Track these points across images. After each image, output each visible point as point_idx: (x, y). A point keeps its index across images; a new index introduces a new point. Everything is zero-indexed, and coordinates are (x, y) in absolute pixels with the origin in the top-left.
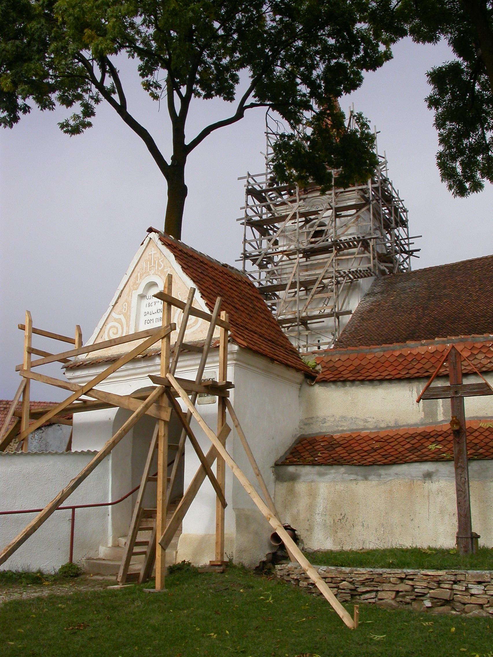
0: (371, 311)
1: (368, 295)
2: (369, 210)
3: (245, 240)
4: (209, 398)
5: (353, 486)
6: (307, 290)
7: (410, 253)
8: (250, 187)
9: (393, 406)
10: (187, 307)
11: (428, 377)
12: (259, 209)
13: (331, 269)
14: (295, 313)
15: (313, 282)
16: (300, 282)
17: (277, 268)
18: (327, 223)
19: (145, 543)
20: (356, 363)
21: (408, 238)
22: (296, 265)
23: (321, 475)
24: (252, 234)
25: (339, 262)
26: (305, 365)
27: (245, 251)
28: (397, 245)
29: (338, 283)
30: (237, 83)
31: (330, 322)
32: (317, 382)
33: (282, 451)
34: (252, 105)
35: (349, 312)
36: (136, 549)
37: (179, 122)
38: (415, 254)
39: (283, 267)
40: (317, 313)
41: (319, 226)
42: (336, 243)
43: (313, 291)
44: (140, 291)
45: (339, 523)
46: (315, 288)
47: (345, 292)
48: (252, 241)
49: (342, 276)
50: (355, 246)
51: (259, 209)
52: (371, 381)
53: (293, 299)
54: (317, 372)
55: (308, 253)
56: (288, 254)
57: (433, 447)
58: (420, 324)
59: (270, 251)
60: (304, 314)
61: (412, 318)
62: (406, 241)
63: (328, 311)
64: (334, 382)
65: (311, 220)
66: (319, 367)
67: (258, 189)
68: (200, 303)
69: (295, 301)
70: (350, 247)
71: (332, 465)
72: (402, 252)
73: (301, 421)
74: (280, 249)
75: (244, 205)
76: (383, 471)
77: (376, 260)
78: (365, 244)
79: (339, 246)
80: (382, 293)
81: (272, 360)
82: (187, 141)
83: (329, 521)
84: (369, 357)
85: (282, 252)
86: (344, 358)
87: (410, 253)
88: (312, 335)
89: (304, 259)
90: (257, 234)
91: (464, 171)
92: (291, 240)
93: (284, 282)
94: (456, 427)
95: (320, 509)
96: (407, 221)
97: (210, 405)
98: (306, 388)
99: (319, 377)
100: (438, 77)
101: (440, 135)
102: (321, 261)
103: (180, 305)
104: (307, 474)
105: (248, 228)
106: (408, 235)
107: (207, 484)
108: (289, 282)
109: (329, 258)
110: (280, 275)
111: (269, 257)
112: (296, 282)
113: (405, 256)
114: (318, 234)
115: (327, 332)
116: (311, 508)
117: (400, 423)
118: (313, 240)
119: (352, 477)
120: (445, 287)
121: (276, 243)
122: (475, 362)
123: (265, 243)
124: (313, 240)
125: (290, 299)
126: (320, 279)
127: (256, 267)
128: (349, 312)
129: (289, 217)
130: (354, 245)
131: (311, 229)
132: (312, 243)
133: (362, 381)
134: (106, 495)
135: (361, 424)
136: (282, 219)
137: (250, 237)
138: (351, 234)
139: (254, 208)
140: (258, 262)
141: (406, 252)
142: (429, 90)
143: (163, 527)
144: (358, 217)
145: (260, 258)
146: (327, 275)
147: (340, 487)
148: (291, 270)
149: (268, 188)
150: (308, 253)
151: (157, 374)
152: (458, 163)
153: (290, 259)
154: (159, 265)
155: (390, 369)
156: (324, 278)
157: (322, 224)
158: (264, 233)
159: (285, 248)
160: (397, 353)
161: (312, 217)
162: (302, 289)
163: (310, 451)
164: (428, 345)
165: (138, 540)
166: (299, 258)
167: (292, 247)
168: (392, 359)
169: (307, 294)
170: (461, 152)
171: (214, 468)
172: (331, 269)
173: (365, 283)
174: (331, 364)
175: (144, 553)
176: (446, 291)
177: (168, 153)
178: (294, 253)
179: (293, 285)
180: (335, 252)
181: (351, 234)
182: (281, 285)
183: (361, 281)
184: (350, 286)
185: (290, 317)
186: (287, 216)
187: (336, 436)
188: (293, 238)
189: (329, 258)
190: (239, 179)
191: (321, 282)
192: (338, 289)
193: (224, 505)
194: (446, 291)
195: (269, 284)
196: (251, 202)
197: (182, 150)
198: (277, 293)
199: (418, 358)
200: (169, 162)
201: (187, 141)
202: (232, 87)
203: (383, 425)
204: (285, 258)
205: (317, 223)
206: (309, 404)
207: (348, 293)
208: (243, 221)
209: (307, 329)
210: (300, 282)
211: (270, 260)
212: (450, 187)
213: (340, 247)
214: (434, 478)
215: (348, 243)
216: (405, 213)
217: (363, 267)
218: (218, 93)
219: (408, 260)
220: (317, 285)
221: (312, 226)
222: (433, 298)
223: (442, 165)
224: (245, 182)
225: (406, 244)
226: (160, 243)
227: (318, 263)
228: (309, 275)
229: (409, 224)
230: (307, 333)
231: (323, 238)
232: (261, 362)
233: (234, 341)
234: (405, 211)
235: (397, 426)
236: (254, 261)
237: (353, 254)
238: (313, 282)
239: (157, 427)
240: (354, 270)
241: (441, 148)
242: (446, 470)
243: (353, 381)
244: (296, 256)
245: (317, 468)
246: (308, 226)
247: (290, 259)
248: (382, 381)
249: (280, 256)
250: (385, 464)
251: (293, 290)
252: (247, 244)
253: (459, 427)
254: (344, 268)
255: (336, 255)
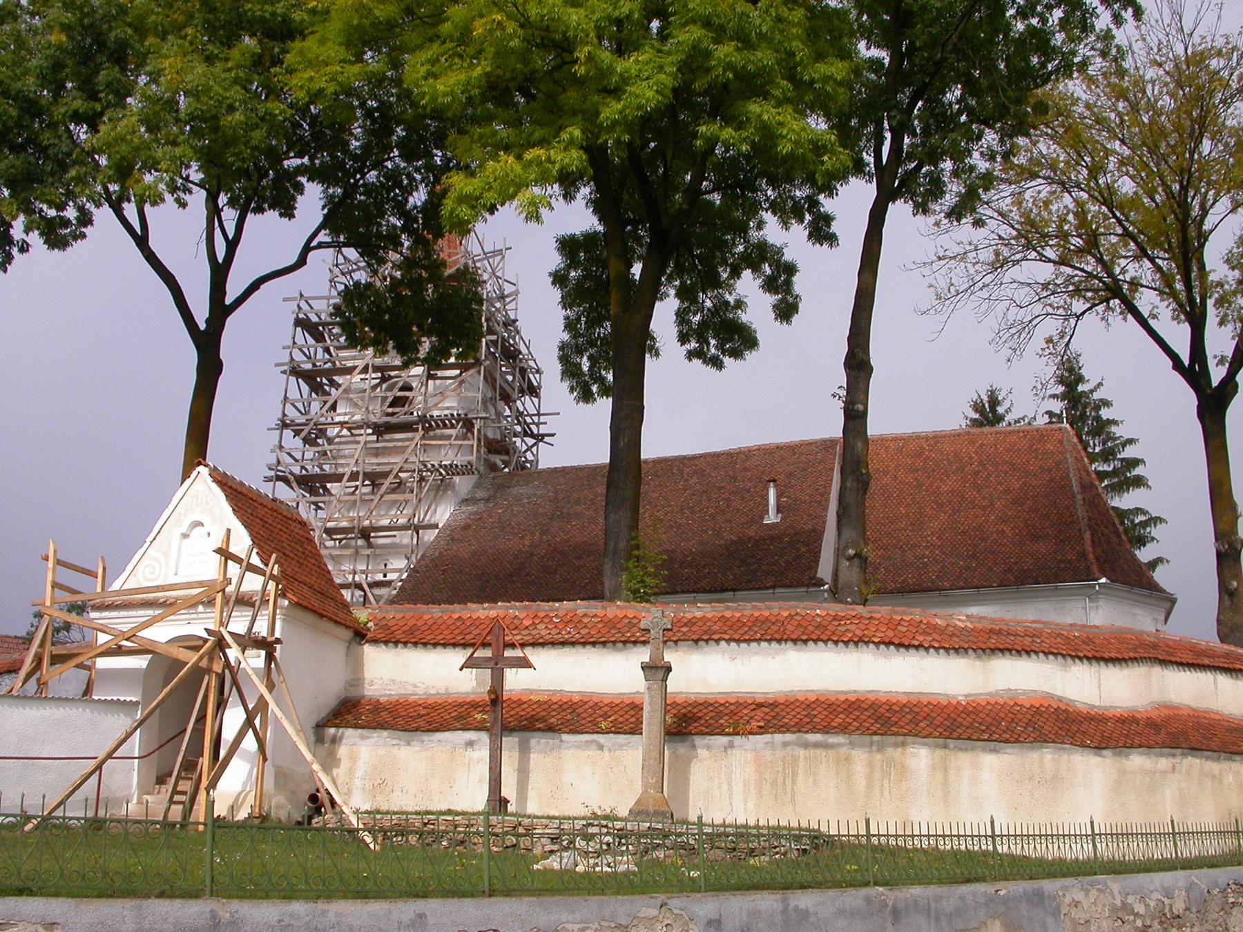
0: (466, 527)
1: (465, 501)
2: (479, 372)
3: (286, 398)
4: (255, 651)
5: (395, 750)
6: (375, 485)
7: (540, 438)
8: (301, 316)
9: (440, 672)
10: (245, 564)
11: (473, 645)
12: (312, 350)
13: (413, 459)
14: (352, 520)
15: (385, 475)
16: (365, 474)
17: (332, 447)
18: (414, 385)
19: (184, 793)
20: (411, 623)
21: (539, 414)
22: (361, 446)
23: (363, 738)
24: (298, 389)
25: (426, 448)
26: (356, 620)
27: (284, 415)
28: (519, 423)
29: (422, 479)
30: (302, 194)
31: (405, 538)
32: (367, 642)
33: (324, 713)
34: (320, 246)
35: (436, 526)
36: (177, 798)
37: (220, 272)
38: (546, 439)
39: (342, 447)
40: (385, 522)
41: (401, 389)
42: (423, 419)
43: (384, 488)
44: (184, 529)
45: (380, 786)
46: (387, 483)
47: (432, 494)
48: (297, 401)
49: (428, 470)
50: (453, 426)
51: (312, 350)
52: (425, 644)
53: (352, 498)
54: (369, 630)
55: (381, 430)
56: (351, 427)
57: (479, 716)
58: (532, 555)
59: (322, 420)
60: (367, 523)
61: (524, 545)
62: (536, 419)
63: (402, 521)
64: (386, 643)
65: (391, 377)
66: (370, 624)
67: (314, 319)
68: (256, 560)
69: (355, 501)
70: (445, 426)
71: (375, 728)
72: (526, 434)
73: (347, 682)
74: (337, 419)
75: (290, 343)
76: (426, 737)
77: (483, 450)
78: (468, 424)
79: (428, 425)
80: (487, 500)
81: (322, 616)
82: (228, 301)
83: (369, 785)
84: (426, 617)
85: (342, 424)
86: (398, 616)
87: (540, 438)
88: (376, 556)
89: (374, 438)
90: (305, 388)
91: (591, 368)
92: (356, 405)
93: (341, 470)
94: (493, 696)
95: (360, 772)
96: (539, 387)
97: (255, 660)
98: (355, 646)
99: (370, 635)
100: (568, 246)
101: (567, 318)
102: (399, 444)
103: (238, 560)
104: (349, 737)
105: (293, 379)
106: (538, 411)
107: (250, 737)
108: (347, 471)
109: (412, 439)
110: (334, 458)
111: (320, 430)
112: (358, 472)
113: (530, 441)
114: (398, 402)
115: (398, 553)
116: (351, 772)
117: (451, 691)
118: (390, 410)
119: (395, 742)
120: (578, 502)
121: (334, 408)
122: (536, 631)
123: (315, 407)
124: (390, 410)
125: (347, 498)
126: (395, 472)
127: (298, 442)
128: (436, 526)
129: (357, 370)
130: (452, 425)
131: (389, 394)
132: (388, 415)
133: (415, 644)
134: (132, 749)
135: (410, 689)
136: (349, 371)
137: (293, 394)
138: (448, 408)
139: (306, 350)
140: (303, 434)
141: (532, 436)
142: (555, 260)
143: (209, 774)
144: (462, 382)
145: (307, 429)
146: (406, 466)
147: (382, 751)
148: (353, 455)
149: (329, 319)
150: (381, 430)
151: (212, 627)
152: (585, 359)
153: (352, 435)
154: (207, 504)
155: (446, 632)
156: (401, 470)
157: (408, 388)
158: (316, 388)
159: (347, 418)
160: (456, 616)
161: (393, 373)
162: (367, 482)
163: (351, 711)
164: (491, 609)
165: (179, 789)
166: (367, 435)
167: (357, 417)
168: (449, 622)
169: (373, 493)
170: (592, 343)
171: (257, 722)
172: (413, 459)
173: (463, 484)
174: (384, 622)
175: (183, 803)
176: (579, 508)
177: (201, 315)
178: (360, 427)
179: (354, 476)
180: (421, 432)
181: (448, 408)
182: (335, 474)
183: (457, 479)
184: (439, 486)
185: (344, 524)
186: (355, 368)
187: (383, 700)
188: (360, 403)
189: (412, 439)
190: (285, 300)
191: (397, 476)
192: (420, 488)
193: (265, 760)
194: (579, 508)
195: (317, 470)
196: (300, 340)
197: (221, 310)
198: (329, 485)
199: (477, 623)
200: (202, 326)
201: (228, 301)
202: (294, 199)
203: (433, 692)
204: (345, 432)
205: (400, 385)
206: (356, 664)
207: (436, 495)
208: (286, 368)
209: (370, 545)
210: (365, 474)
211: (322, 433)
212: (572, 389)
213: (431, 425)
214: (476, 747)
215: (443, 421)
216: (537, 376)
217: (460, 460)
218: (272, 207)
219: (534, 449)
220: (390, 479)
221: (390, 389)
222: (558, 517)
223: (564, 359)
224: (293, 306)
225: (534, 423)
226: (210, 479)
227: (394, 447)
228: (379, 464)
229: (543, 393)
230: (368, 552)
231: (406, 408)
232: (311, 618)
233: (284, 596)
234: (538, 371)
235: (447, 693)
236: (297, 433)
237: (449, 437)
238: (385, 475)
239: (207, 677)
240: (447, 463)
241: (566, 337)
242: (484, 737)
243: (405, 643)
244: (362, 432)
245: (360, 731)
246: (384, 386)
247: (352, 435)
248: (435, 645)
249: (337, 430)
250: (428, 731)
251: (353, 484)
252: (288, 405)
253: (496, 698)
254: (433, 459)
255: (423, 438)
